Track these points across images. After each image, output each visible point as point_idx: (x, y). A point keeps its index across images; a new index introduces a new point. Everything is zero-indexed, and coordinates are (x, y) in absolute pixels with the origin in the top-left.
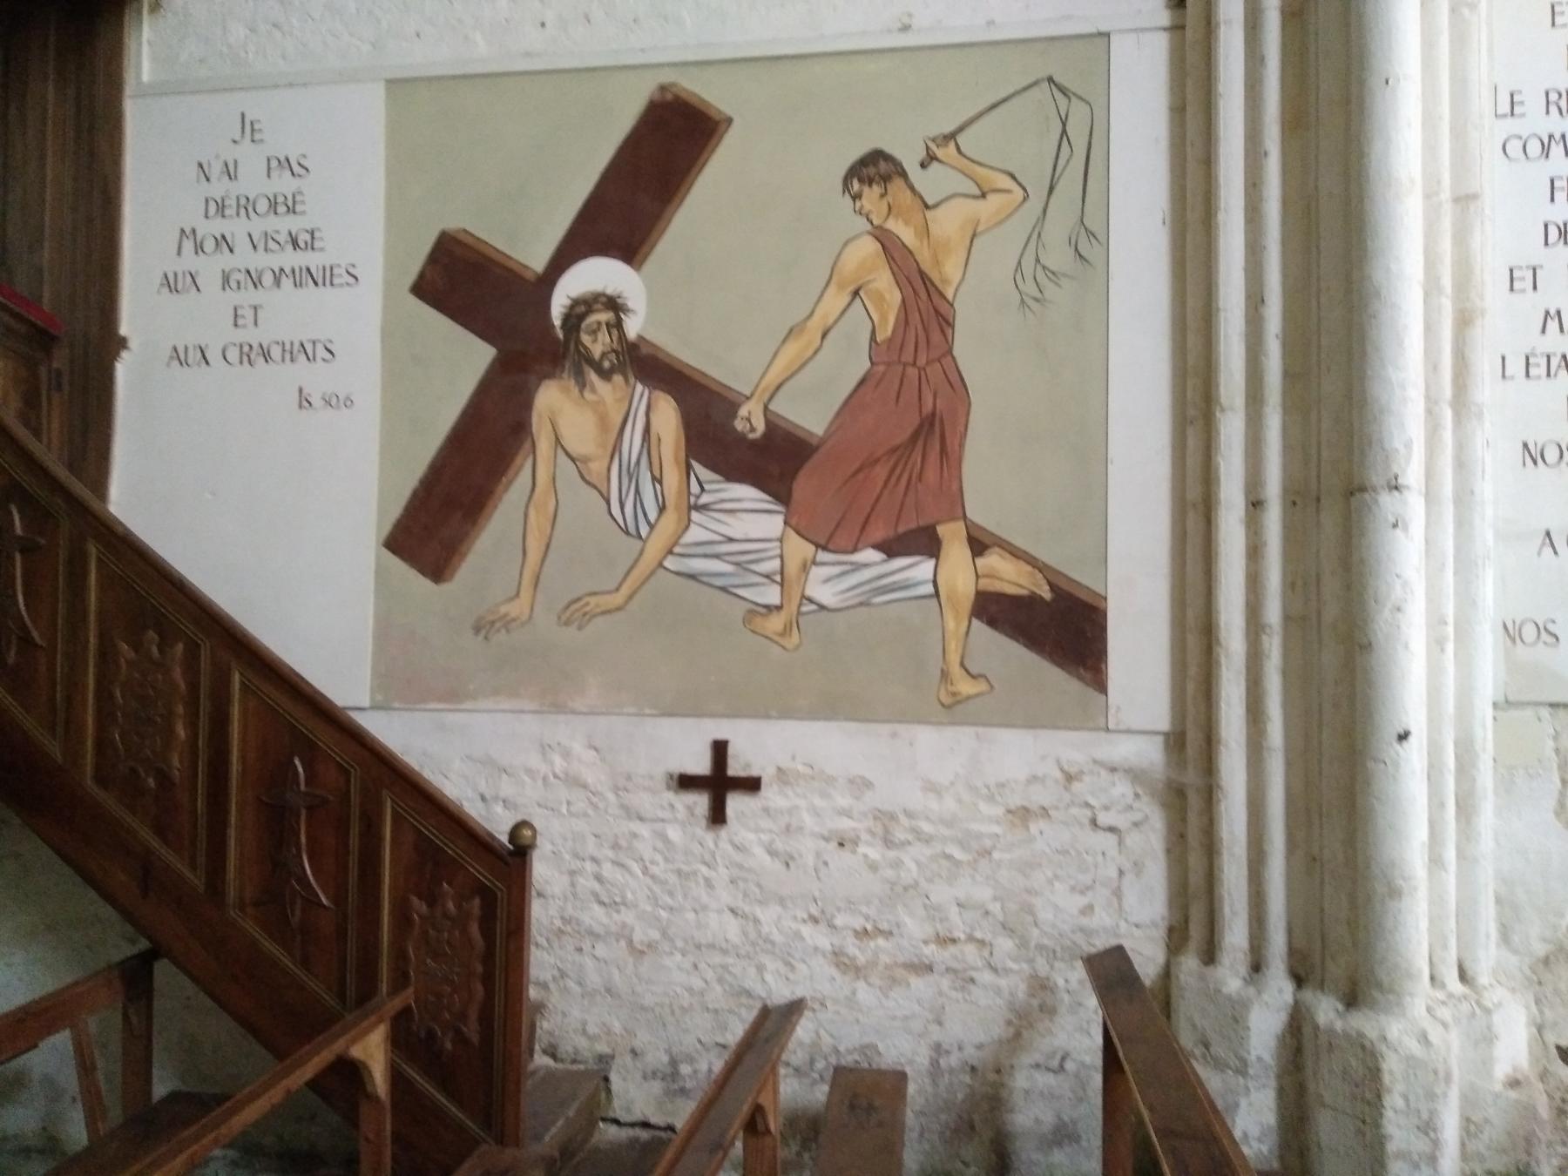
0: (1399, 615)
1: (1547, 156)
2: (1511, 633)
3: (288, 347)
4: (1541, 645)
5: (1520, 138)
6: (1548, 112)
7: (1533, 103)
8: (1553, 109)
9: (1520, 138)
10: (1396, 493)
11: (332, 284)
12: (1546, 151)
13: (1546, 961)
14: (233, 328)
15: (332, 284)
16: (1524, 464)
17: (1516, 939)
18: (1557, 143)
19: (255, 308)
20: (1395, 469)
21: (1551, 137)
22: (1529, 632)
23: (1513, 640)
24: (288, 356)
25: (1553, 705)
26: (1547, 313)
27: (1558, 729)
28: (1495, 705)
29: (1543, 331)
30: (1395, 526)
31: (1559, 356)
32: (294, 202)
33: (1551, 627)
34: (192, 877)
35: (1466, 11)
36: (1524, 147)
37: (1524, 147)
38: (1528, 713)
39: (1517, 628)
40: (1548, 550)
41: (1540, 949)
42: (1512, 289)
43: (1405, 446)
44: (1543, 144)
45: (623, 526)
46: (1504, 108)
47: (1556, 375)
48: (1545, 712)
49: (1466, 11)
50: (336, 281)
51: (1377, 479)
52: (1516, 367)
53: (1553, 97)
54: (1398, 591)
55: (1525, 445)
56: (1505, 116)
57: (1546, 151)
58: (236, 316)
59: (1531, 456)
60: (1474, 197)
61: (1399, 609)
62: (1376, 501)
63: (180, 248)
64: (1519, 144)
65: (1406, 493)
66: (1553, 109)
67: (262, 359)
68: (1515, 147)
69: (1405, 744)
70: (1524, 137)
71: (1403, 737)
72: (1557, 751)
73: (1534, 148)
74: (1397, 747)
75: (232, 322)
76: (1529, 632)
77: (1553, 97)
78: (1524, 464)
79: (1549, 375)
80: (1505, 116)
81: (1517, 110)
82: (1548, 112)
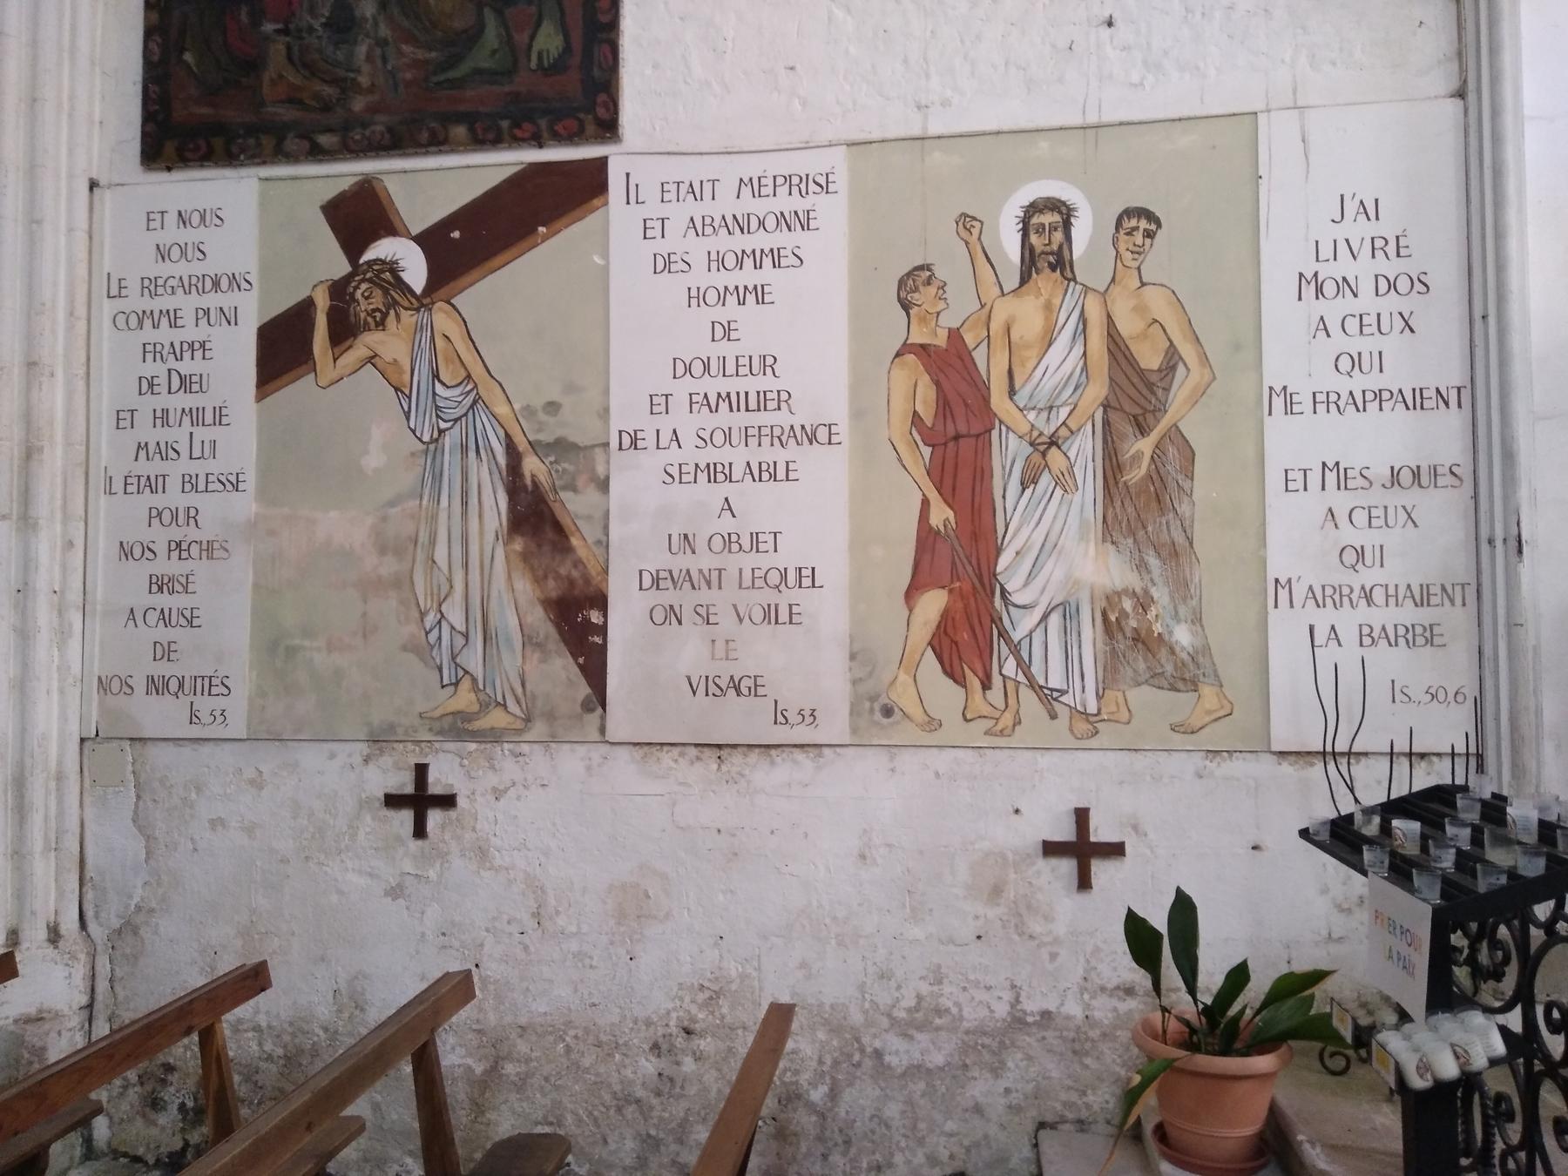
3: (1391, 591)
13: (119, 932)
17: (103, 915)
22: (116, 685)
24: (1392, 601)
25: (131, 739)
34: (210, 1107)
40: (131, 623)
41: (116, 923)
45: (1349, 783)
46: (114, 292)
50: (1351, 484)
52: (118, 486)
55: (121, 543)
63: (137, 457)
64: (124, 317)
67: (1363, 602)
68: (121, 319)
73: (133, 321)
76: (116, 685)
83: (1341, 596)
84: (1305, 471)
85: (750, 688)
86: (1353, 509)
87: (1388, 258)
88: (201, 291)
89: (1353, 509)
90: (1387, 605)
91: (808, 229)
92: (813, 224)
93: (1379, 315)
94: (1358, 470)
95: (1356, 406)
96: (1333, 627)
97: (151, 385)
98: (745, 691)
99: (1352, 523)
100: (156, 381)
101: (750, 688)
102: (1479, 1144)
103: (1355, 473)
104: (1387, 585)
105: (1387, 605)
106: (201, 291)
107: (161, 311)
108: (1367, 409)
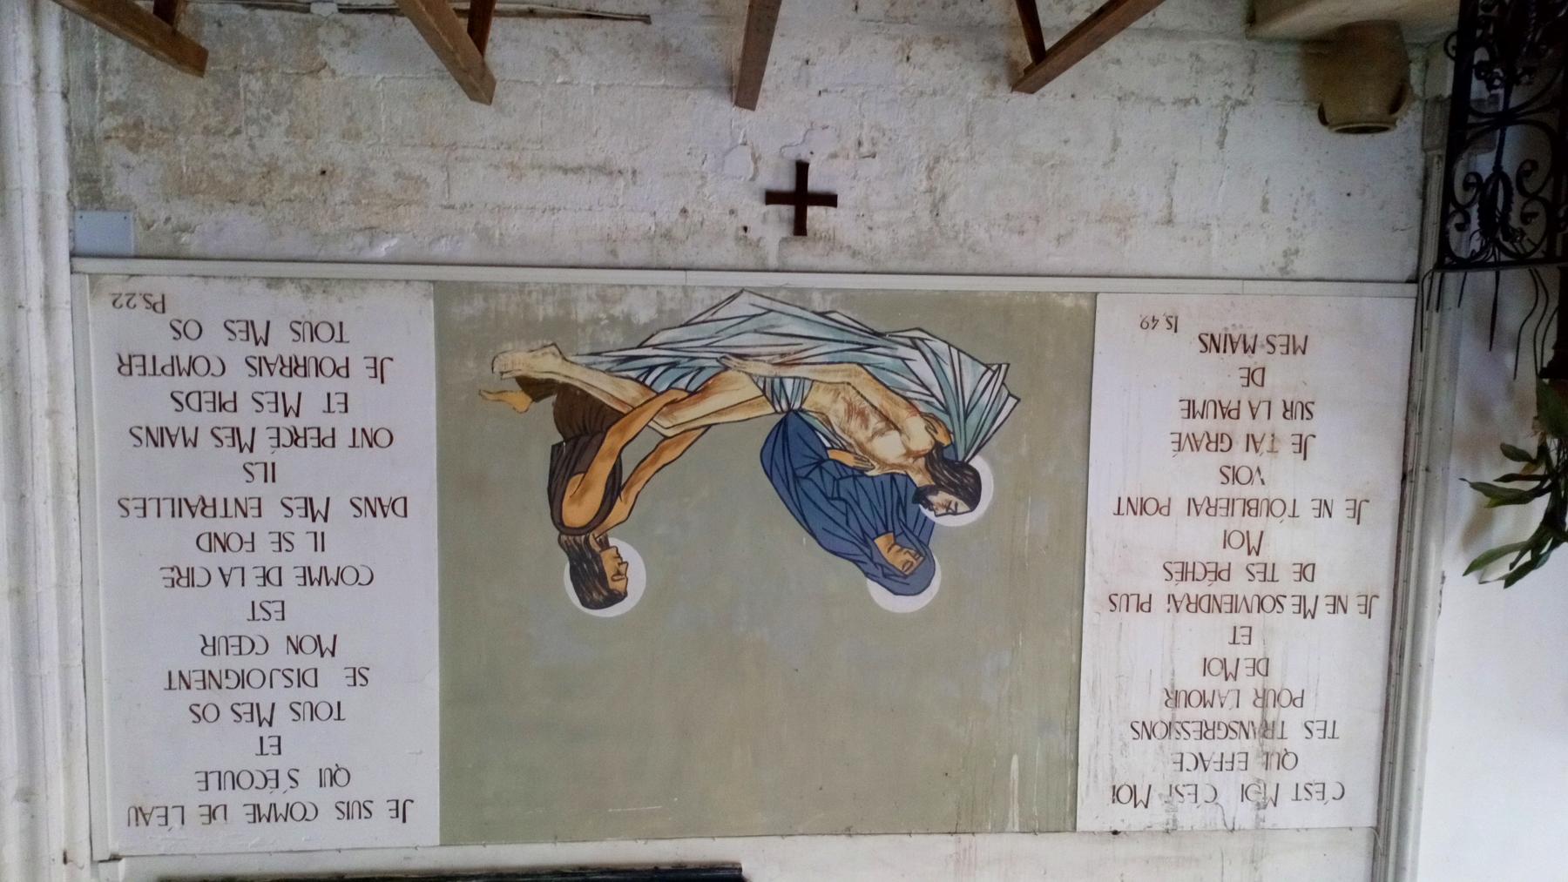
16: (1347, 597)
78: (1347, 597)
83: (291, 366)
84: (1119, 513)
85: (1219, 729)
86: (368, 584)
87: (225, 818)
88: (1204, 723)
89: (368, 584)
90: (1194, 563)
91: (1321, 501)
92: (1317, 504)
93: (227, 654)
94: (243, 721)
95: (1174, 600)
96: (227, 584)
97: (266, 576)
98: (1223, 727)
99: (314, 805)
100: (261, 581)
101: (1219, 729)
102: (1560, 15)
103: (297, 513)
104: (1193, 580)
105: (1194, 563)
106: (1204, 723)
107: (1212, 706)
108: (331, 431)
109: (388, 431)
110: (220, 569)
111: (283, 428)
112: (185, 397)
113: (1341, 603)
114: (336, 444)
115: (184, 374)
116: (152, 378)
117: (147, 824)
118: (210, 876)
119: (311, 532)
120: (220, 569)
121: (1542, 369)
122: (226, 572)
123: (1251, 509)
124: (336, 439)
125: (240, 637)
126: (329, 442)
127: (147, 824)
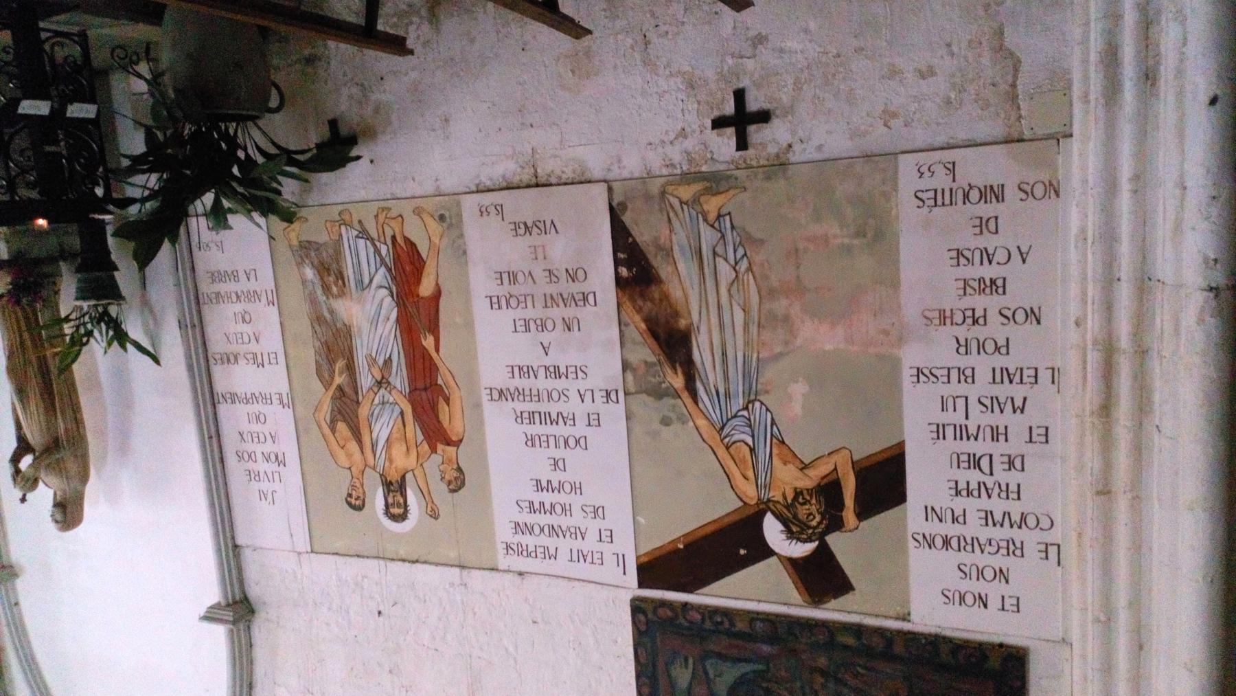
0: (1214, 194)
1: (1023, 514)
2: (1054, 189)
4: (1031, 183)
5: (1041, 529)
6: (1022, 543)
7: (1032, 550)
8: (1018, 545)
9: (1041, 529)
10: (1214, 285)
11: (969, 455)
12: (1023, 518)
14: (600, 413)
15: (969, 455)
16: (1040, 308)
18: (1015, 522)
19: (1031, 441)
20: (1214, 303)
21: (1020, 527)
22: (1039, 190)
23: (1051, 184)
26: (1022, 411)
27: (1017, 123)
28: (1071, 136)
29: (1025, 399)
30: (1216, 261)
31: (1014, 382)
32: (987, 519)
33: (1023, 196)
35: (1103, 618)
36: (1038, 523)
37: (1038, 523)
38: (1040, 132)
39: (1048, 194)
40: (1024, 250)
42: (1047, 429)
43: (1204, 320)
44: (1026, 524)
46: (1053, 551)
47: (1017, 369)
48: (1027, 134)
49: (1103, 618)
51: (1225, 295)
52: (1045, 376)
53: (1018, 552)
54: (1214, 211)
56: (1051, 544)
57: (1023, 518)
58: (1047, 435)
59: (1035, 315)
60: (1099, 493)
61: (1214, 198)
62: (1228, 277)
65: (1204, 285)
66: (1018, 545)
68: (1045, 523)
69: (1211, 94)
70: (1038, 528)
71: (1213, 101)
72: (1019, 108)
73: (1031, 521)
74: (1218, 92)
75: (1050, 431)
77: (1018, 552)
78: (1040, 308)
79: (1022, 369)
80: (1051, 544)
81: (1043, 547)
82: (1022, 543)
104: (952, 324)
109: (1003, 247)
110: (579, 391)
111: (957, 309)
112: (1030, 187)
113: (1035, 315)
114: (987, 322)
115: (556, 491)
116: (493, 294)
117: (1002, 412)
118: (1211, 422)
119: (982, 510)
120: (579, 391)
121: (174, 240)
122: (582, 393)
123: (551, 373)
124: (987, 318)
125: (491, 389)
126: (981, 321)
127: (1002, 412)
